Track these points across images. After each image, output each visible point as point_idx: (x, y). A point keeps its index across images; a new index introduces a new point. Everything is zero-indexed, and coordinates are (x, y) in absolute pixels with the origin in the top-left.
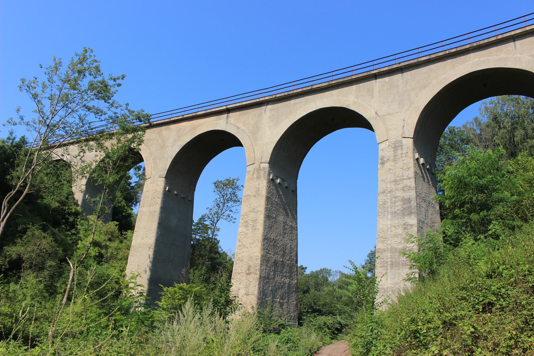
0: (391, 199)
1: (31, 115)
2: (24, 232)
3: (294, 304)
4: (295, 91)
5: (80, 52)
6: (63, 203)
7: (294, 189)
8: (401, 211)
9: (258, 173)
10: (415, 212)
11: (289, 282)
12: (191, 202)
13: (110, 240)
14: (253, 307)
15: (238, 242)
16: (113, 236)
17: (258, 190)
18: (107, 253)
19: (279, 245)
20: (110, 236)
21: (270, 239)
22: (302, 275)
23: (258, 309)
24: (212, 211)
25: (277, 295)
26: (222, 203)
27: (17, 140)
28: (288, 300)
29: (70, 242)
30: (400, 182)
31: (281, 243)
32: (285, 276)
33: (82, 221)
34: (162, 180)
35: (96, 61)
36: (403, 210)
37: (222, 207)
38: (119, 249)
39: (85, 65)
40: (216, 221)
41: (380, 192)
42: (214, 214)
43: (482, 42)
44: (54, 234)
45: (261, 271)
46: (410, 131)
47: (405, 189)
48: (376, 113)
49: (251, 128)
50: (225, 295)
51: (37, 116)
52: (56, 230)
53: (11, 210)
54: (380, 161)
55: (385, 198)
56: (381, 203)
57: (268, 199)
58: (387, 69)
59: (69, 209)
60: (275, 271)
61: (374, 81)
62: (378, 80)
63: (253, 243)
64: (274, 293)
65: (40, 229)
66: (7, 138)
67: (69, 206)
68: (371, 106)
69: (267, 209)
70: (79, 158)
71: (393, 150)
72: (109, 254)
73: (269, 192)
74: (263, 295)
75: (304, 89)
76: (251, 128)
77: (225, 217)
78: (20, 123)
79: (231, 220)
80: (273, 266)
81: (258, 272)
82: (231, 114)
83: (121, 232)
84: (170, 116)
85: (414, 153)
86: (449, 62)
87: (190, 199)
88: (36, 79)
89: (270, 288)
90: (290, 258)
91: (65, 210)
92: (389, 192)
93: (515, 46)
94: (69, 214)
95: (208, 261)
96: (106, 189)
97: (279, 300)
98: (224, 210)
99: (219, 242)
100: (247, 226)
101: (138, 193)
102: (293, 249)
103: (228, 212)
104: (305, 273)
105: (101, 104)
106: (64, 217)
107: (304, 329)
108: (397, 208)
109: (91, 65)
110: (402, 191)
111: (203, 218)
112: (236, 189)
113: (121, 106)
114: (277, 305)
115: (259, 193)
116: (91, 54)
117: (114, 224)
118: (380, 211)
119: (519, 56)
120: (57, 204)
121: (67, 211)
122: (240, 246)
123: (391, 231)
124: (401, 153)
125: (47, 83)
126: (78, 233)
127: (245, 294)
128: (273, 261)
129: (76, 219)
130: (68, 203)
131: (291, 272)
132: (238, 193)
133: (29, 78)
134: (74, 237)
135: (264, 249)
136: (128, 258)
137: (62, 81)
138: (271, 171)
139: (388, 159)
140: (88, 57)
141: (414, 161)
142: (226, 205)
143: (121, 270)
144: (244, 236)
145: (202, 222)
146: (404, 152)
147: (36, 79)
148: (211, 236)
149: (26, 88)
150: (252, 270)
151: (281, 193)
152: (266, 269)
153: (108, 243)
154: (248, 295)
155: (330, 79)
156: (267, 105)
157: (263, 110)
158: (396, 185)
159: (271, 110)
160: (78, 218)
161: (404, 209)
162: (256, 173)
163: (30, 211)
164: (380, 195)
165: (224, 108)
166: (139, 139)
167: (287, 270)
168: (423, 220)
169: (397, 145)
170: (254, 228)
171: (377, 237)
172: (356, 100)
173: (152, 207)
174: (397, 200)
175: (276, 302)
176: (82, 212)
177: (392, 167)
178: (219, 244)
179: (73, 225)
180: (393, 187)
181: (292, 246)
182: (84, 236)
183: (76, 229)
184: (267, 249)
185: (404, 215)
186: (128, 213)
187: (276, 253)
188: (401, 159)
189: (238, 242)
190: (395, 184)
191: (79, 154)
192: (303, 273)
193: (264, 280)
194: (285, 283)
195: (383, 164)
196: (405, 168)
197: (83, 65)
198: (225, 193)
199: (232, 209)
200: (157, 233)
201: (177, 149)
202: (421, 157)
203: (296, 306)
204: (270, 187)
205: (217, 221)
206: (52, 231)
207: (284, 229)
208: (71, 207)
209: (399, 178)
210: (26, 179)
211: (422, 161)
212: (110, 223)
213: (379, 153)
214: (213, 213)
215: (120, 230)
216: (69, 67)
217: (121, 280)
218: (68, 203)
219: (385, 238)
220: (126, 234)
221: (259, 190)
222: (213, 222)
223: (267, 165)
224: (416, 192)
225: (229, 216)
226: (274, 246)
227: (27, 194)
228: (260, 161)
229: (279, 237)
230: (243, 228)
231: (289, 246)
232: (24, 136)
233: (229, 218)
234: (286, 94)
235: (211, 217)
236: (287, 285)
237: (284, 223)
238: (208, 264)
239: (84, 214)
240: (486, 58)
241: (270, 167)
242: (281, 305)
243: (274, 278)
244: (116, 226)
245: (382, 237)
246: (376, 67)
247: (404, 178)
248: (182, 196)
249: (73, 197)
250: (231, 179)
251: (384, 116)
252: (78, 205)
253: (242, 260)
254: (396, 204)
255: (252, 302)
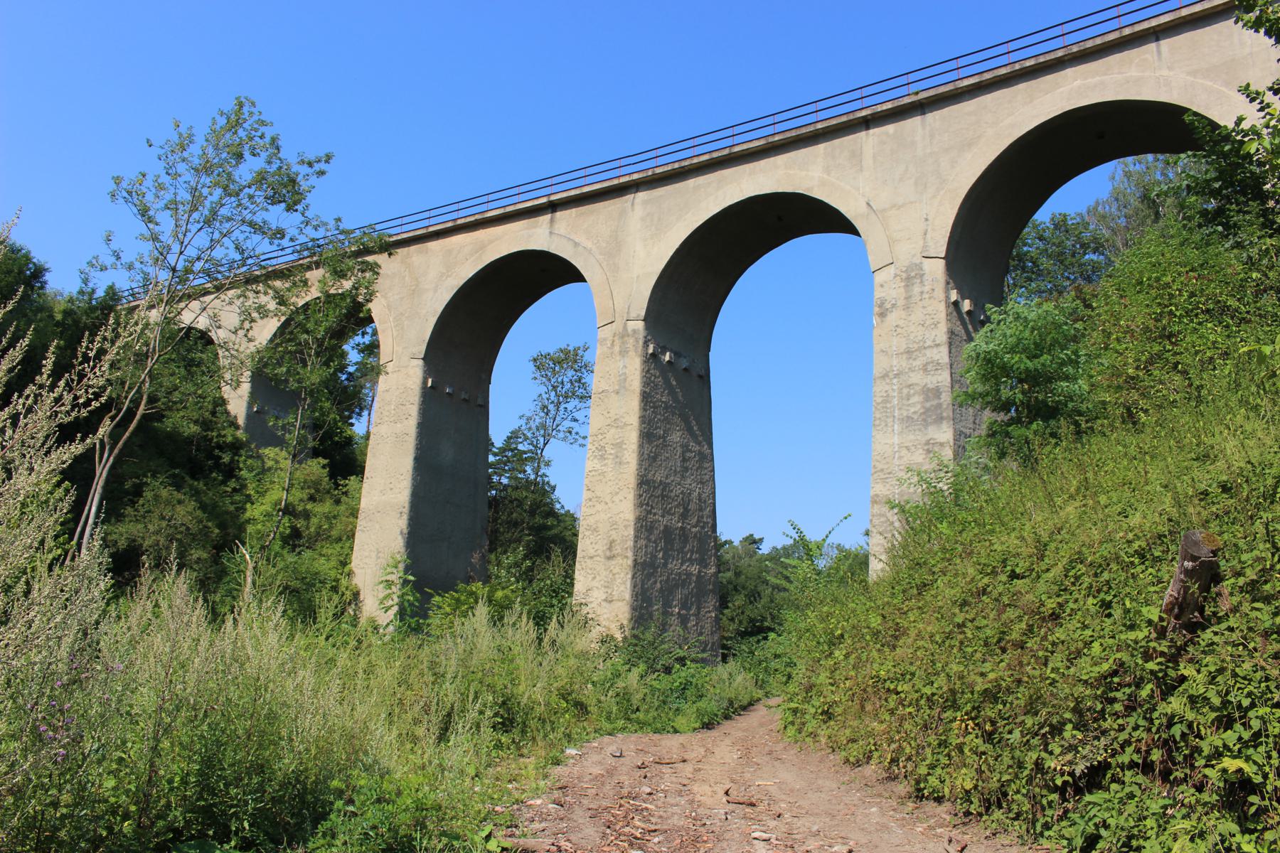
0: (900, 390)
1: (135, 247)
2: (138, 492)
3: (711, 617)
4: (695, 160)
5: (230, 106)
6: (206, 425)
7: (703, 372)
8: (921, 414)
9: (623, 343)
10: (948, 416)
11: (699, 572)
12: (484, 408)
13: (312, 498)
14: (622, 627)
15: (585, 492)
16: (318, 491)
17: (623, 380)
18: (308, 528)
19: (673, 494)
20: (313, 491)
21: (654, 482)
22: (751, 557)
23: (633, 629)
24: (531, 422)
25: (673, 600)
26: (553, 402)
27: (100, 293)
28: (699, 608)
29: (232, 508)
30: (917, 353)
31: (677, 490)
32: (690, 559)
33: (249, 462)
34: (418, 366)
35: (263, 123)
36: (924, 413)
37: (553, 412)
38: (335, 517)
39: (241, 133)
40: (541, 445)
41: (878, 375)
42: (538, 430)
43: (1089, 44)
44: (196, 494)
45: (636, 550)
46: (939, 241)
47: (929, 367)
48: (868, 204)
49: (604, 245)
50: (560, 602)
51: (147, 248)
52: (201, 485)
53: (116, 451)
54: (876, 309)
55: (887, 388)
56: (879, 400)
57: (646, 398)
58: (889, 106)
59: (219, 436)
60: (666, 551)
61: (863, 134)
62: (871, 131)
63: (617, 493)
64: (667, 594)
65: (170, 485)
66: (79, 293)
67: (219, 430)
68: (859, 189)
69: (643, 420)
70: (241, 333)
71: (903, 284)
72: (312, 530)
73: (647, 382)
74: (643, 601)
75: (715, 155)
76: (604, 245)
77: (561, 435)
78: (114, 267)
79: (576, 440)
80: (661, 539)
81: (630, 554)
82: (558, 214)
83: (336, 480)
84: (426, 223)
85: (947, 291)
86: (1022, 87)
87: (480, 401)
88: (144, 176)
89: (658, 585)
90: (698, 521)
91: (212, 439)
92: (897, 376)
93: (1159, 52)
94: (220, 447)
95: (529, 535)
96: (305, 399)
97: (677, 610)
98: (558, 419)
99: (554, 488)
100: (602, 458)
101: (362, 387)
102: (705, 501)
103: (567, 424)
104: (760, 552)
105: (276, 216)
106: (210, 456)
107: (732, 664)
108: (912, 410)
109: (253, 133)
110: (921, 372)
111: (514, 436)
112: (583, 370)
113: (325, 224)
114: (674, 620)
115: (627, 385)
116: (253, 109)
117: (319, 463)
118: (878, 416)
119: (1165, 73)
120: (194, 429)
121: (215, 440)
122: (590, 500)
123: (900, 458)
124: (920, 290)
125: (165, 179)
126: (244, 486)
127: (605, 600)
128: (662, 528)
129: (236, 458)
130: (216, 423)
131: (702, 550)
132: (587, 378)
133: (130, 175)
134: (237, 498)
135: (641, 505)
136: (353, 535)
137: (196, 170)
138: (649, 337)
139: (894, 306)
140: (246, 116)
141: (947, 307)
142: (563, 406)
143: (341, 562)
144: (599, 478)
145: (514, 446)
146: (927, 288)
147: (144, 176)
148: (532, 477)
149: (125, 194)
150: (618, 549)
151: (674, 383)
152: (646, 547)
153: (309, 506)
154: (611, 602)
155: (770, 130)
156: (637, 192)
157: (629, 204)
158: (911, 361)
159: (645, 202)
160: (241, 456)
161: (927, 411)
162: (617, 342)
163: (140, 446)
164: (878, 382)
165: (544, 200)
166: (367, 288)
167: (693, 547)
168: (968, 432)
169: (913, 274)
170: (618, 460)
171: (873, 471)
172: (825, 176)
173: (399, 425)
174: (912, 391)
175: (672, 615)
176: (248, 442)
177: (901, 323)
178: (556, 492)
179: (230, 472)
180: (904, 365)
181: (704, 495)
182: (258, 492)
183: (238, 478)
184: (647, 504)
185: (926, 424)
186: (345, 437)
187: (666, 512)
188: (920, 304)
189: (585, 492)
190: (909, 359)
191: (242, 324)
192: (755, 553)
193: (644, 570)
194: (689, 575)
195: (882, 315)
196: (928, 323)
197: (236, 133)
198: (560, 380)
199: (577, 415)
200: (414, 479)
201: (445, 296)
202: (963, 298)
203: (715, 621)
204: (648, 371)
205: (545, 444)
206: (191, 487)
207: (684, 460)
208: (223, 433)
209: (916, 346)
210: (140, 387)
211: (966, 305)
212: (309, 462)
213: (875, 293)
214: (534, 427)
215: (332, 476)
216: (207, 140)
217: (344, 582)
218: (216, 423)
219: (889, 473)
220: (346, 485)
221: (625, 380)
222: (536, 447)
223: (640, 325)
224: (951, 374)
225: (570, 432)
226: (663, 496)
227: (144, 416)
228: (625, 315)
229: (672, 478)
230: (596, 461)
231: (696, 494)
232: (113, 284)
233: (570, 437)
234: (676, 166)
235: (529, 435)
236: (694, 578)
237: (682, 446)
238: (530, 541)
239: (253, 446)
240: (1098, 78)
241: (647, 327)
242: (684, 621)
243: (665, 565)
244: (324, 467)
245: (882, 470)
246: (867, 102)
247: (926, 345)
248: (463, 396)
249: (226, 410)
250: (571, 348)
251: (884, 210)
252: (237, 427)
253: (595, 530)
254: (911, 402)
255: (620, 616)
